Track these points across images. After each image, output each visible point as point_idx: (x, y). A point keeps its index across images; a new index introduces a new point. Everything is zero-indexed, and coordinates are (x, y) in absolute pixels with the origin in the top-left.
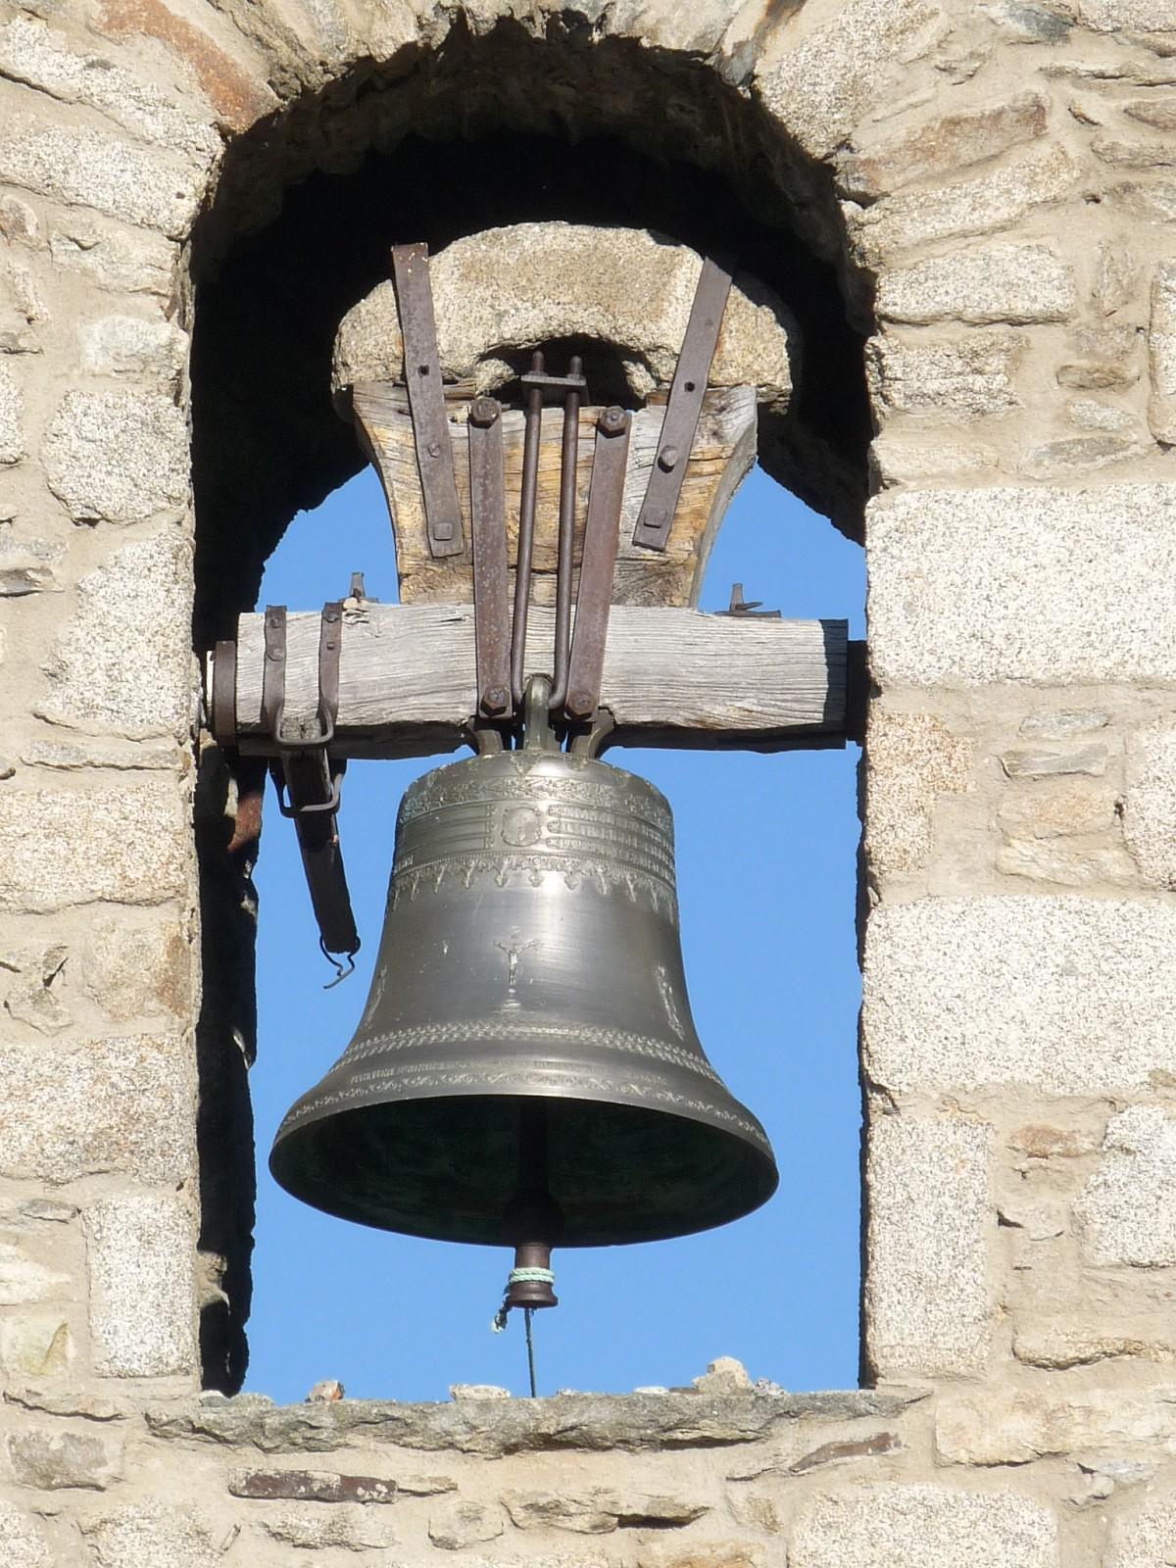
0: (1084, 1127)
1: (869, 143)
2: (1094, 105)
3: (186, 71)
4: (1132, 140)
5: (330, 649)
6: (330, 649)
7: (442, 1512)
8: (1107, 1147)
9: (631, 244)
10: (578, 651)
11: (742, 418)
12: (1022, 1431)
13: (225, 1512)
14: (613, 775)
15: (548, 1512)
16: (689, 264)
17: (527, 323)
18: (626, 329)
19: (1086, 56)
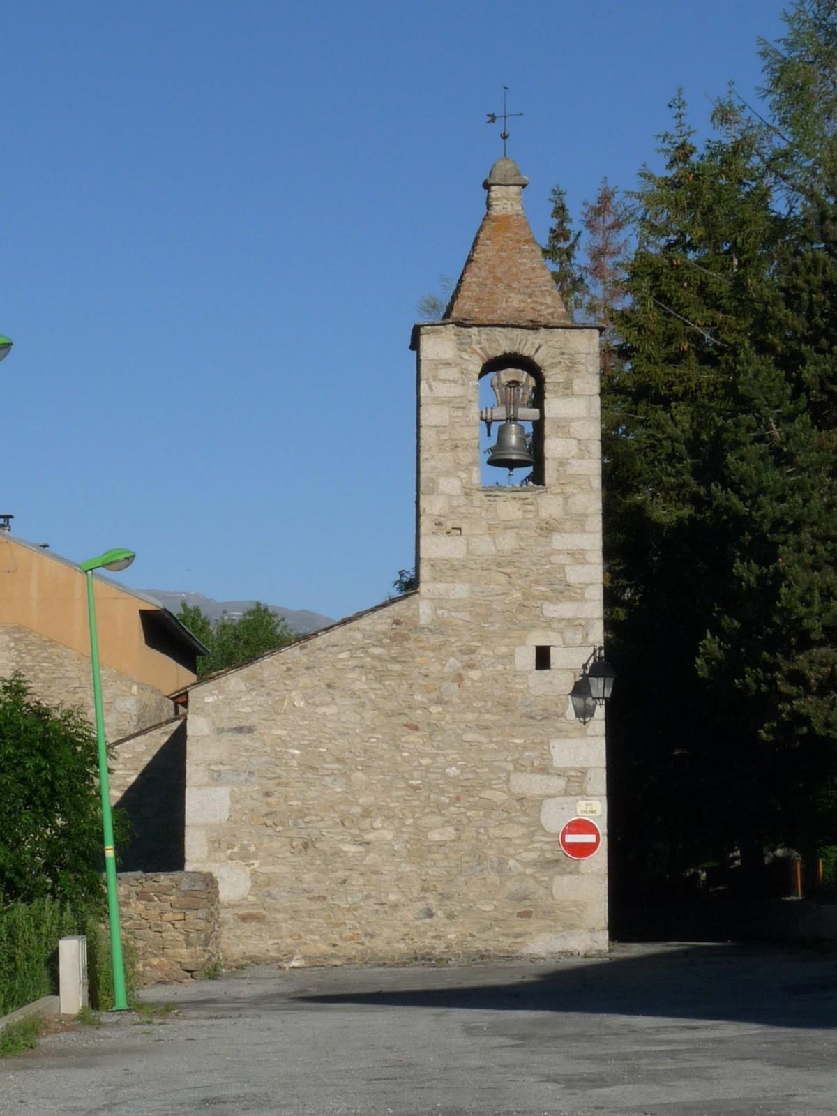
0: (565, 461)
1: (545, 365)
2: (567, 361)
3: (453, 325)
4: (570, 365)
5: (492, 412)
6: (492, 412)
7: (505, 498)
8: (567, 463)
9: (520, 371)
10: (516, 412)
11: (531, 389)
12: (560, 491)
13: (484, 498)
14: (519, 425)
15: (515, 498)
16: (525, 373)
17: (510, 379)
18: (520, 380)
19: (565, 356)
